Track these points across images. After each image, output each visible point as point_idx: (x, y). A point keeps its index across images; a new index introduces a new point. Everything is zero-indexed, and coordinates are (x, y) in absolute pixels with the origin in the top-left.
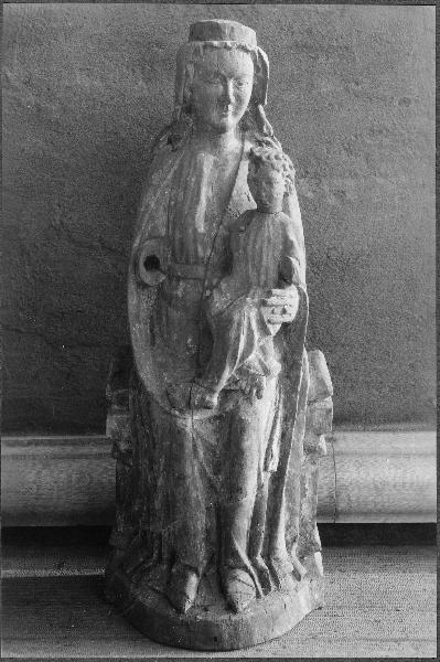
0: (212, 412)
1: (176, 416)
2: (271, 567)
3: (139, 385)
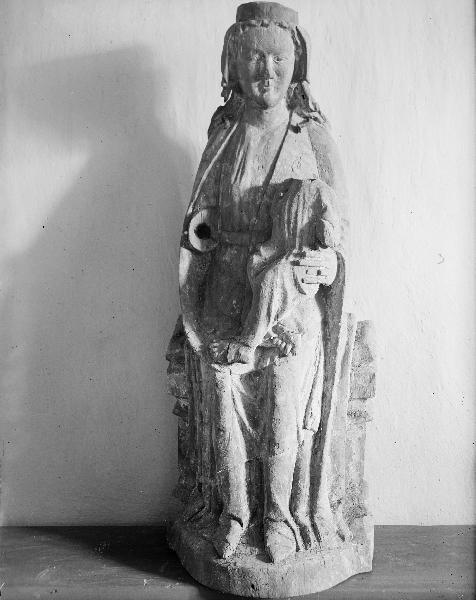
0: (249, 367)
1: (216, 370)
2: (314, 526)
3: (189, 346)
